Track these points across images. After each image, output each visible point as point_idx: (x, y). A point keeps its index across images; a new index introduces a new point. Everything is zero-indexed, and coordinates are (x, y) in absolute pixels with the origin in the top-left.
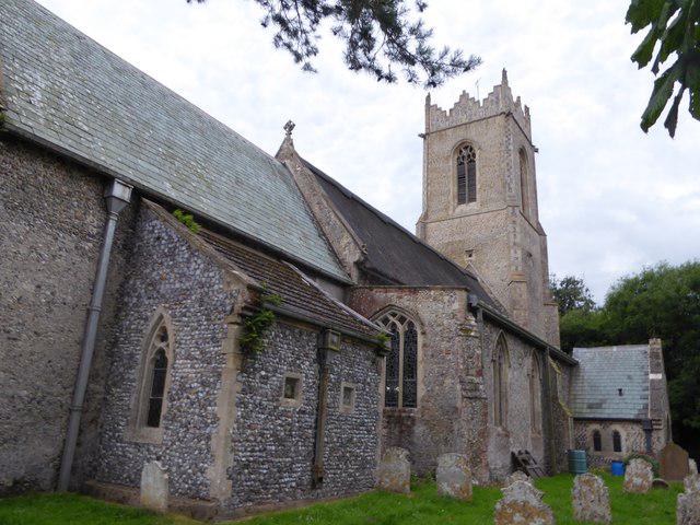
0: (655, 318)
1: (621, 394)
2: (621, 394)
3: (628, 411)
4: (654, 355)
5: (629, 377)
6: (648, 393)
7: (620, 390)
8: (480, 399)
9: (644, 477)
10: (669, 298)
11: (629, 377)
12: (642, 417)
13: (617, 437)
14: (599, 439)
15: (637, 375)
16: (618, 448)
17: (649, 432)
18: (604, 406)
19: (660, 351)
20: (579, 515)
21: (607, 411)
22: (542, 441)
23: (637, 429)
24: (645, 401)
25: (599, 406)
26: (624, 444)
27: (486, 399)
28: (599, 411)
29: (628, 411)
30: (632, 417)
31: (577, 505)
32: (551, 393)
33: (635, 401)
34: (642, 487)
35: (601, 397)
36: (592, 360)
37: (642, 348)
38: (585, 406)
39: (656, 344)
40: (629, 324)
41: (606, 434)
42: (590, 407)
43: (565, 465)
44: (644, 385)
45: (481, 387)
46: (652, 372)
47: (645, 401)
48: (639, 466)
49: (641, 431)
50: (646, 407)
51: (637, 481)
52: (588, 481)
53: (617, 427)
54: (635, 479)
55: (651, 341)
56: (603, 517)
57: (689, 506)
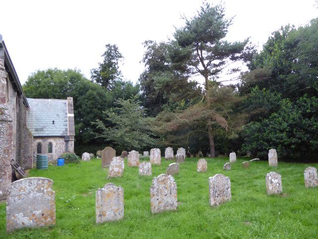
0: (53, 90)
1: (53, 123)
2: (53, 123)
3: (57, 132)
4: (69, 105)
5: (58, 115)
6: (68, 123)
7: (53, 121)
8: (6, 121)
9: (120, 167)
10: (61, 82)
11: (58, 115)
12: (65, 135)
13: (51, 144)
14: (41, 147)
15: (62, 114)
16: (50, 151)
17: (67, 142)
18: (44, 129)
19: (72, 103)
20: (156, 208)
21: (47, 132)
22: (15, 151)
23: (62, 140)
24: (66, 127)
25: (42, 130)
26: (54, 149)
27: (11, 121)
28: (42, 132)
29: (57, 132)
30: (60, 135)
31: (154, 202)
32: (22, 122)
33: (61, 127)
34: (118, 173)
35: (43, 125)
36: (37, 105)
37: (64, 101)
38: (34, 130)
39: (70, 100)
40: (40, 92)
41: (45, 144)
42: (36, 130)
43: (34, 165)
44: (65, 119)
45: (6, 111)
46: (69, 113)
47: (66, 127)
48: (118, 161)
49: (63, 142)
50: (66, 130)
51: (116, 169)
52: (163, 181)
53: (51, 140)
54: (115, 169)
55: (68, 98)
56: (172, 205)
57: (216, 184)
